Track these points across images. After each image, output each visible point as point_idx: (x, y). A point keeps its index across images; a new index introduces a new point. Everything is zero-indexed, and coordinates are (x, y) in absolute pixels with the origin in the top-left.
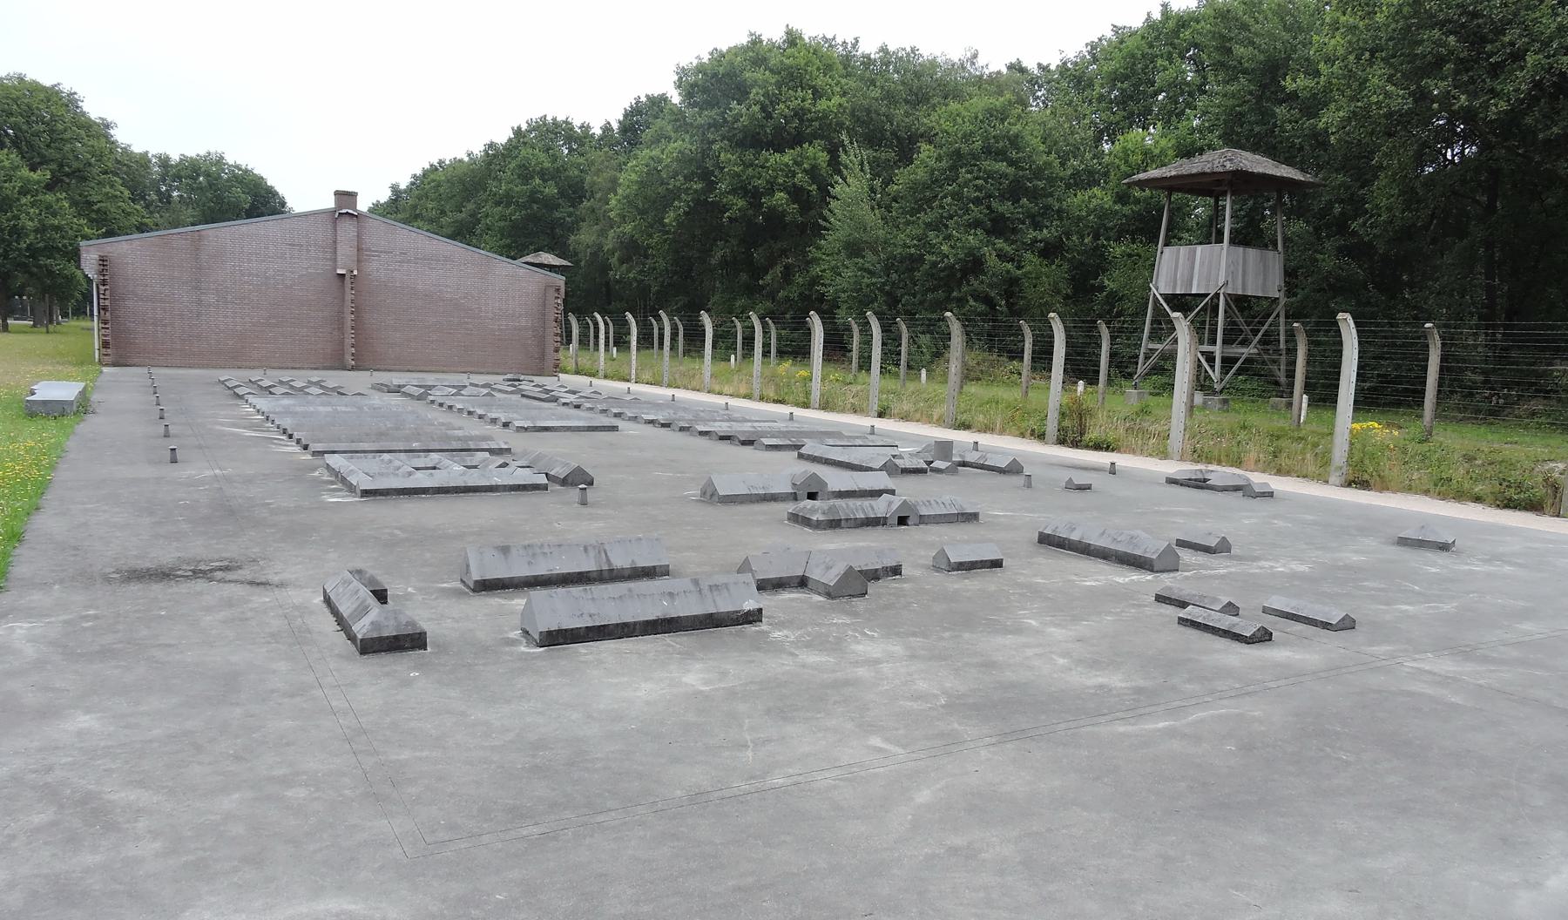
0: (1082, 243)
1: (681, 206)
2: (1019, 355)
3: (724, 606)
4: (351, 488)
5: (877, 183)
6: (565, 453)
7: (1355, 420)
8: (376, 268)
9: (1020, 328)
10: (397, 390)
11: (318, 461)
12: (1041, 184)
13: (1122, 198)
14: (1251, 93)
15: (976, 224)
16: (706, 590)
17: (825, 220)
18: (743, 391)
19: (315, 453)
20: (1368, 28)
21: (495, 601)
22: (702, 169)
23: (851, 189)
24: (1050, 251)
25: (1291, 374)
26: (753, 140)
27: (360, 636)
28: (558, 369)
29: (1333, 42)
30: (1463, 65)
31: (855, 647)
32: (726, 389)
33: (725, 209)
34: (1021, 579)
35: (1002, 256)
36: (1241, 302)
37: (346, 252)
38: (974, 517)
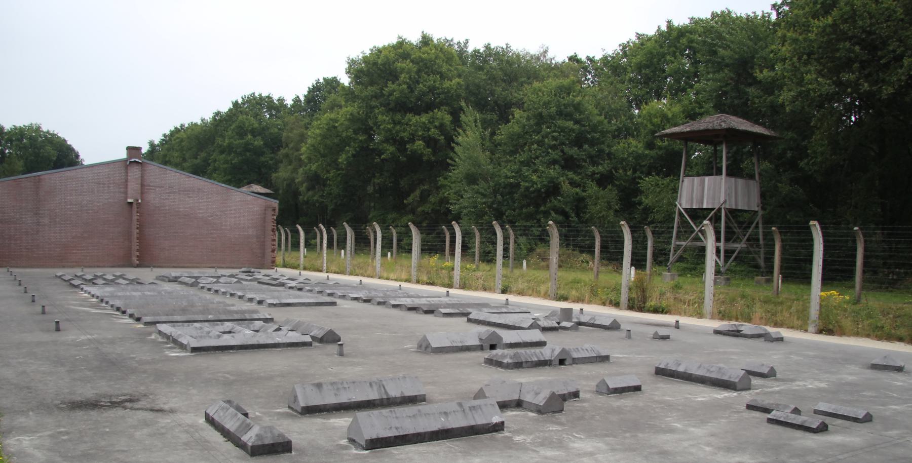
0: (626, 175)
1: (350, 150)
2: (590, 250)
3: (480, 420)
4: (182, 347)
5: (487, 133)
6: (319, 321)
7: (822, 291)
8: (153, 198)
9: (591, 231)
10: (175, 280)
11: (150, 329)
12: (597, 135)
13: (650, 145)
14: (731, 79)
15: (554, 162)
16: (467, 410)
17: (452, 159)
18: (404, 276)
19: (147, 324)
20: (805, 40)
21: (317, 421)
22: (364, 126)
23: (469, 138)
24: (603, 181)
25: (769, 259)
26: (402, 107)
27: (250, 444)
28: (273, 264)
29: (784, 49)
30: (863, 65)
31: (572, 445)
32: (392, 276)
33: (380, 153)
34: (656, 398)
35: (573, 183)
36: (733, 213)
37: (134, 186)
38: (605, 359)
